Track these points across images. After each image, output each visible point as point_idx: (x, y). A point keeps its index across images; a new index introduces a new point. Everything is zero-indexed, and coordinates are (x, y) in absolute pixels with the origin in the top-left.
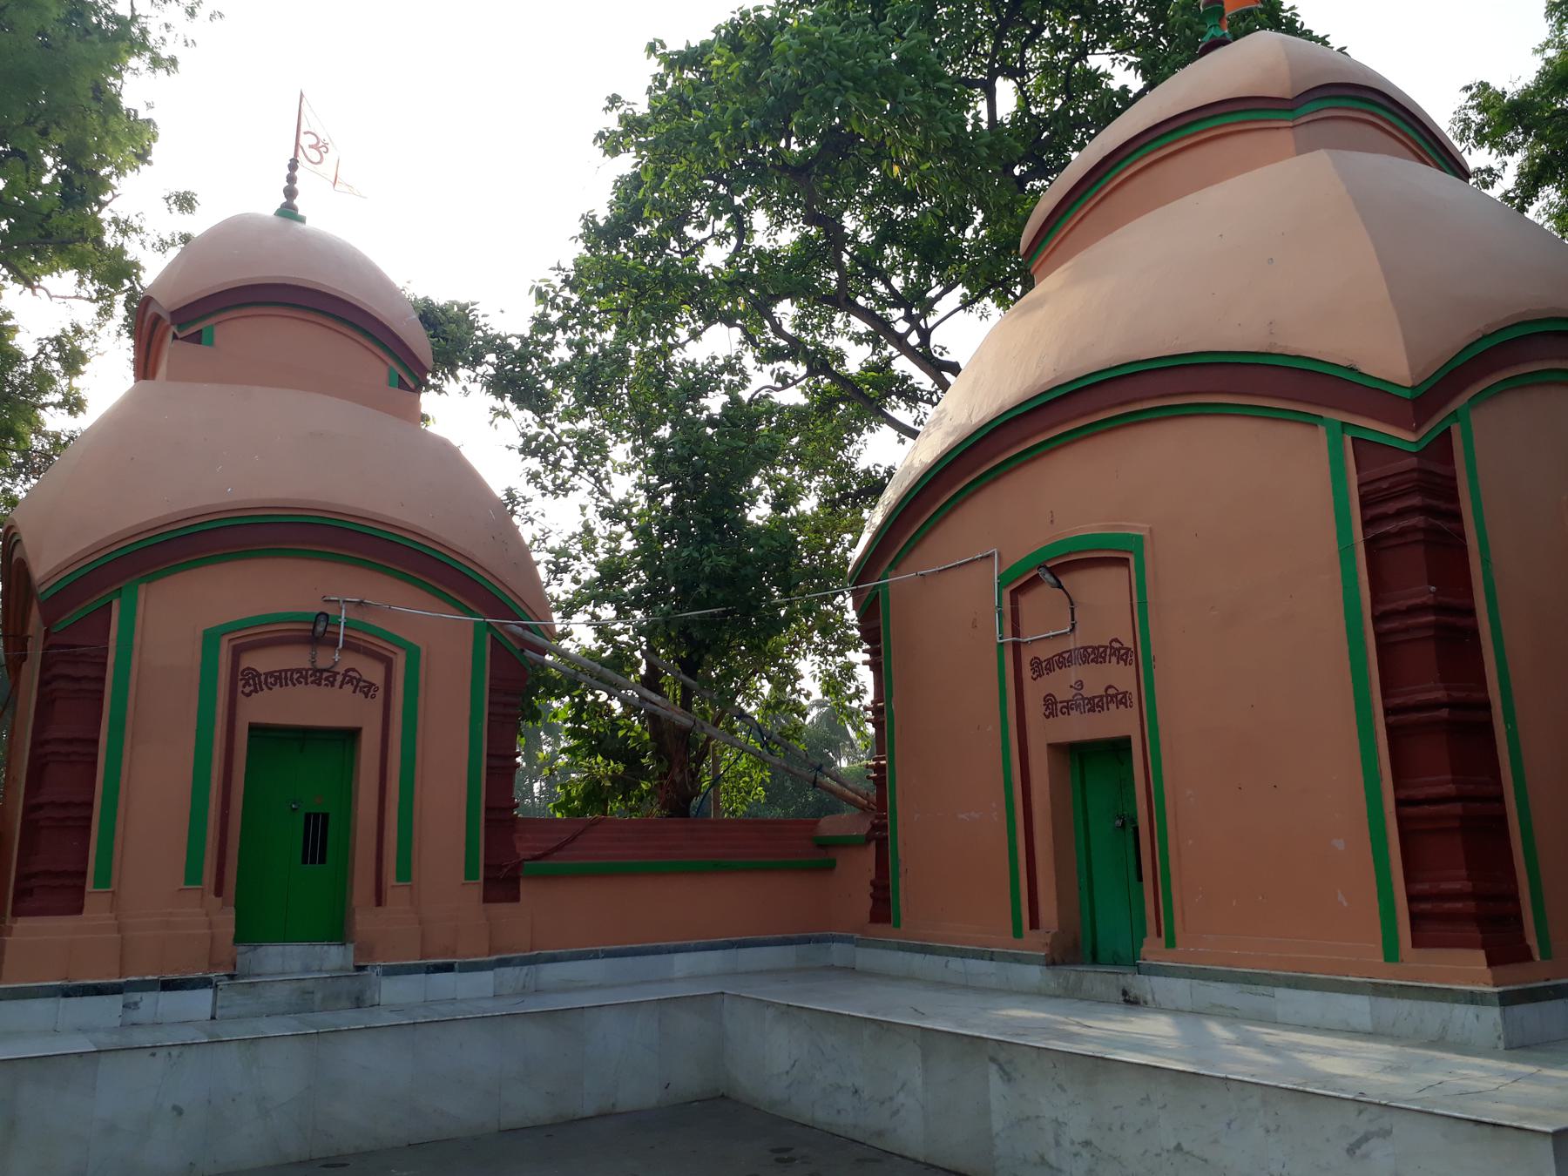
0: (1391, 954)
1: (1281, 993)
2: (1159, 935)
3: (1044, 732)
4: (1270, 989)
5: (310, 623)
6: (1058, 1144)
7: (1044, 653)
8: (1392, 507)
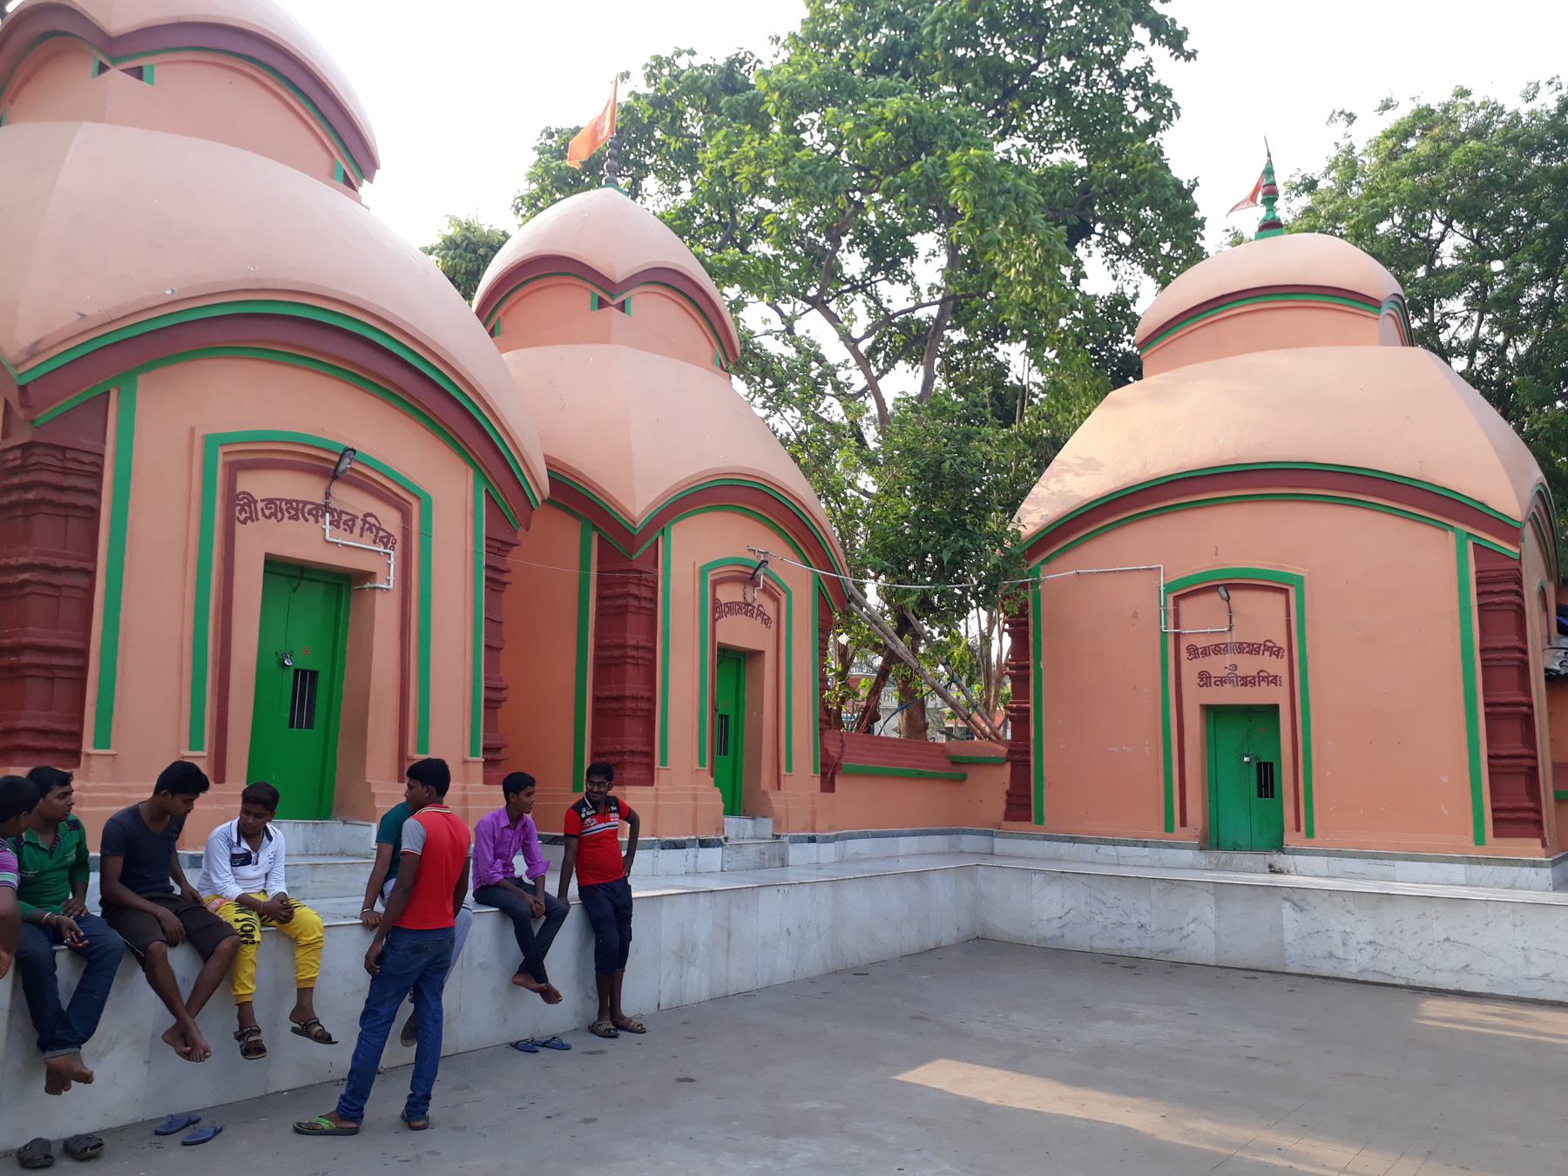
0: (1479, 840)
1: (1399, 864)
2: (1298, 829)
3: (1195, 697)
4: (1391, 862)
5: (336, 453)
6: (1345, 944)
7: (1201, 643)
8: (1497, 588)
